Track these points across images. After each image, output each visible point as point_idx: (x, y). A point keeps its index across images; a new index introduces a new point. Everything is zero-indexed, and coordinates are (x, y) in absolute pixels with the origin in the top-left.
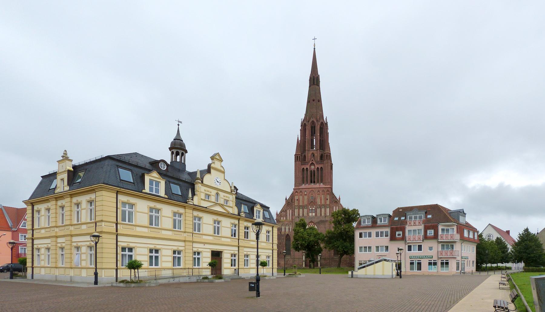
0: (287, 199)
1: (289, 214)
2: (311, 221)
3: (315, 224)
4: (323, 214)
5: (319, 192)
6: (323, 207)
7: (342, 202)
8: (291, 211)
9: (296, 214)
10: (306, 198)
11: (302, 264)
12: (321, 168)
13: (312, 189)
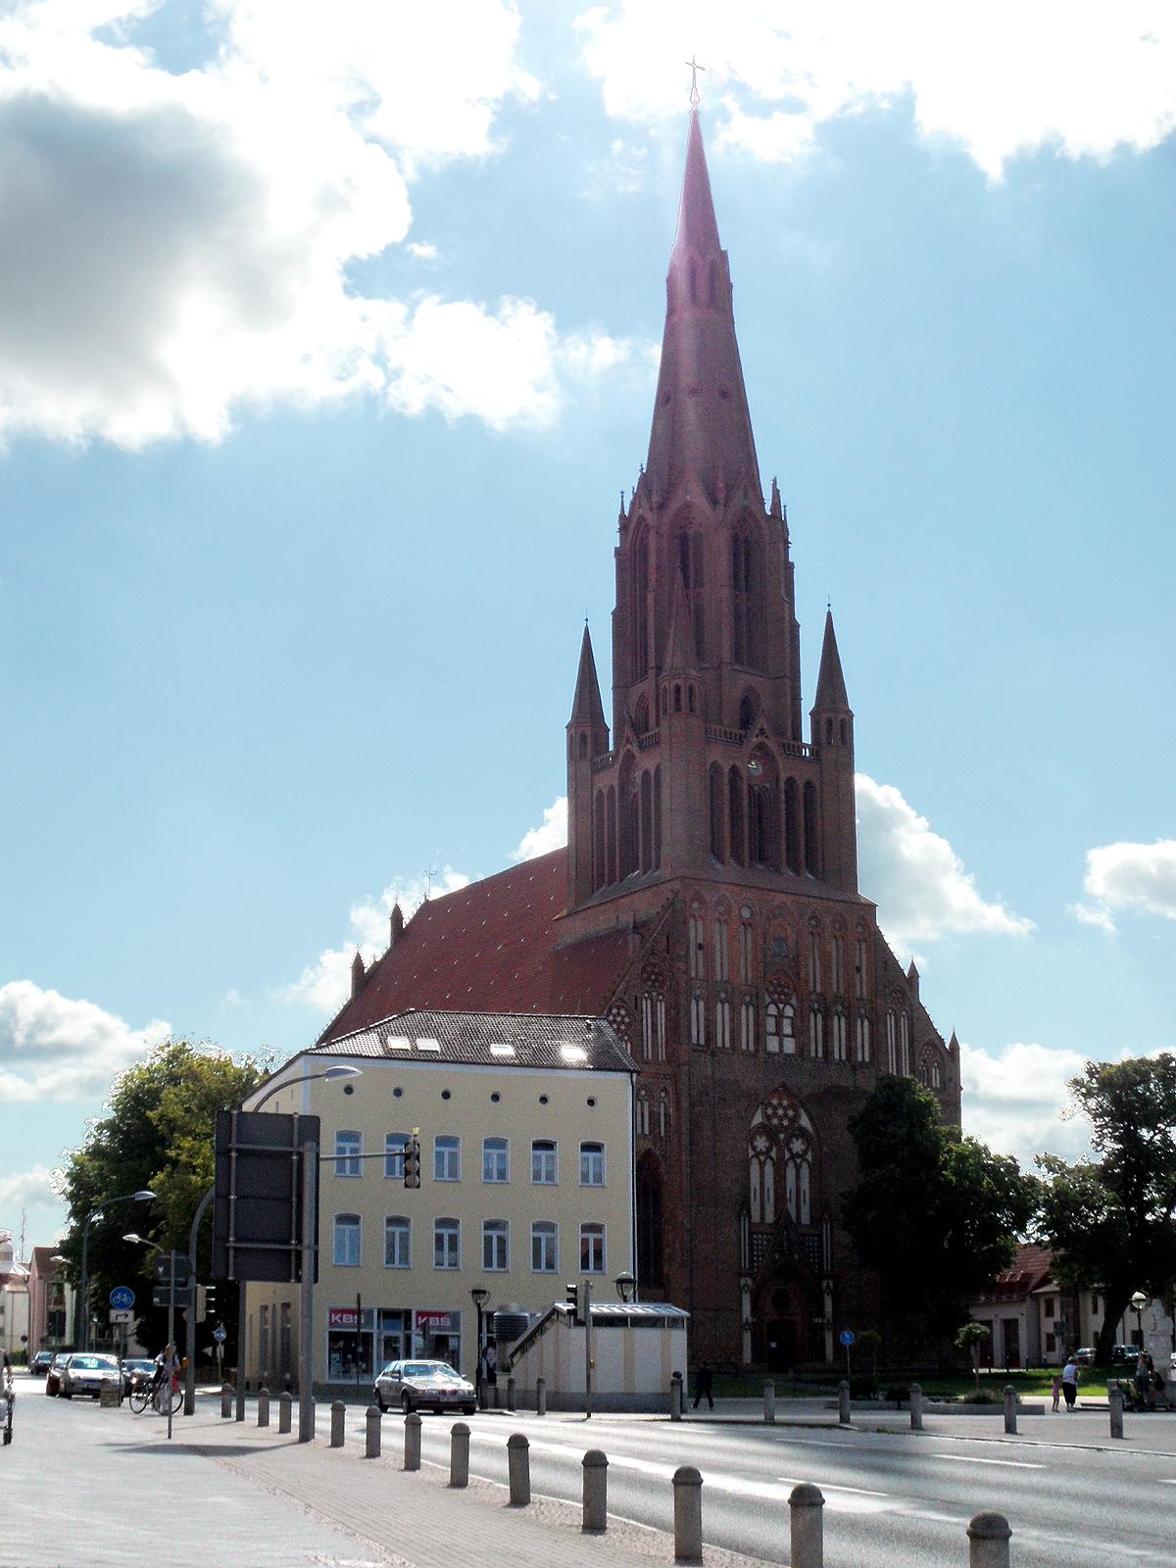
0: (406, 921)
2: (784, 1085)
4: (839, 1052)
8: (661, 1008)
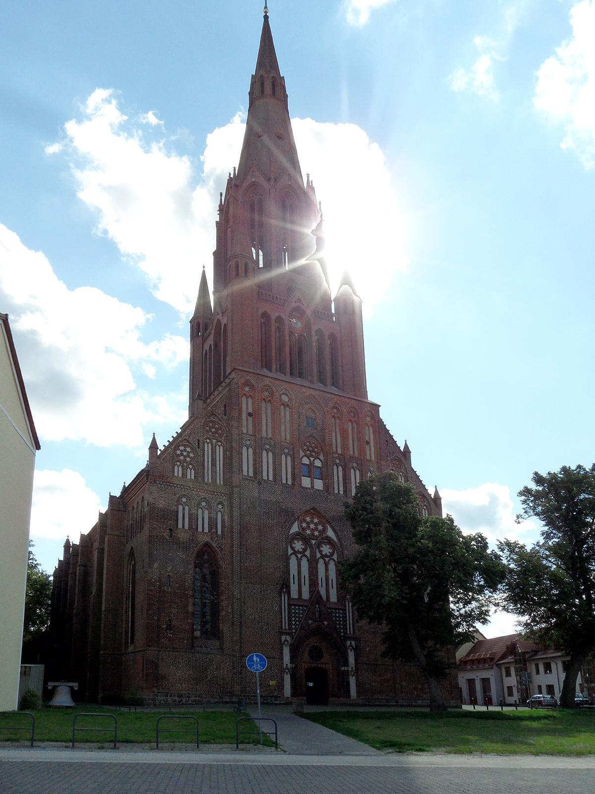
2: (314, 509)
6: (355, 465)
9: (247, 469)
11: (281, 685)
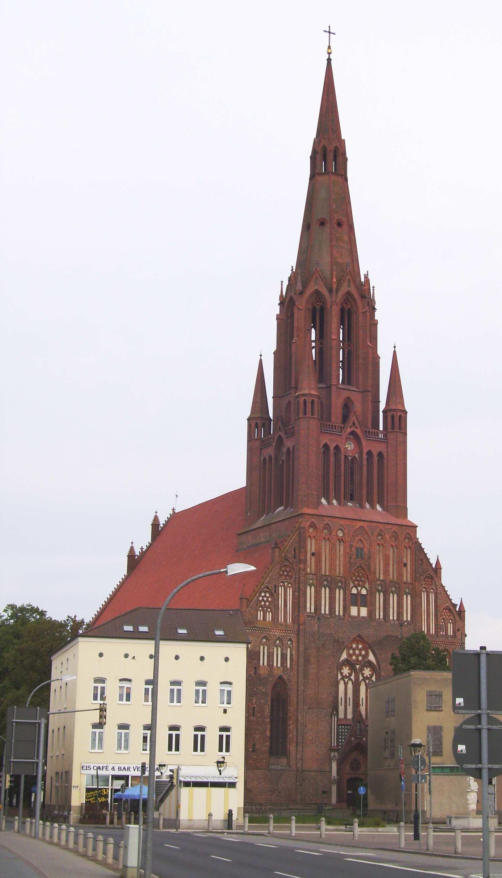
1: (432, 604)
2: (359, 636)
3: (368, 646)
4: (393, 616)
5: (380, 537)
6: (394, 589)
7: (446, 580)
10: (342, 552)
12: (334, 449)
13: (362, 524)
